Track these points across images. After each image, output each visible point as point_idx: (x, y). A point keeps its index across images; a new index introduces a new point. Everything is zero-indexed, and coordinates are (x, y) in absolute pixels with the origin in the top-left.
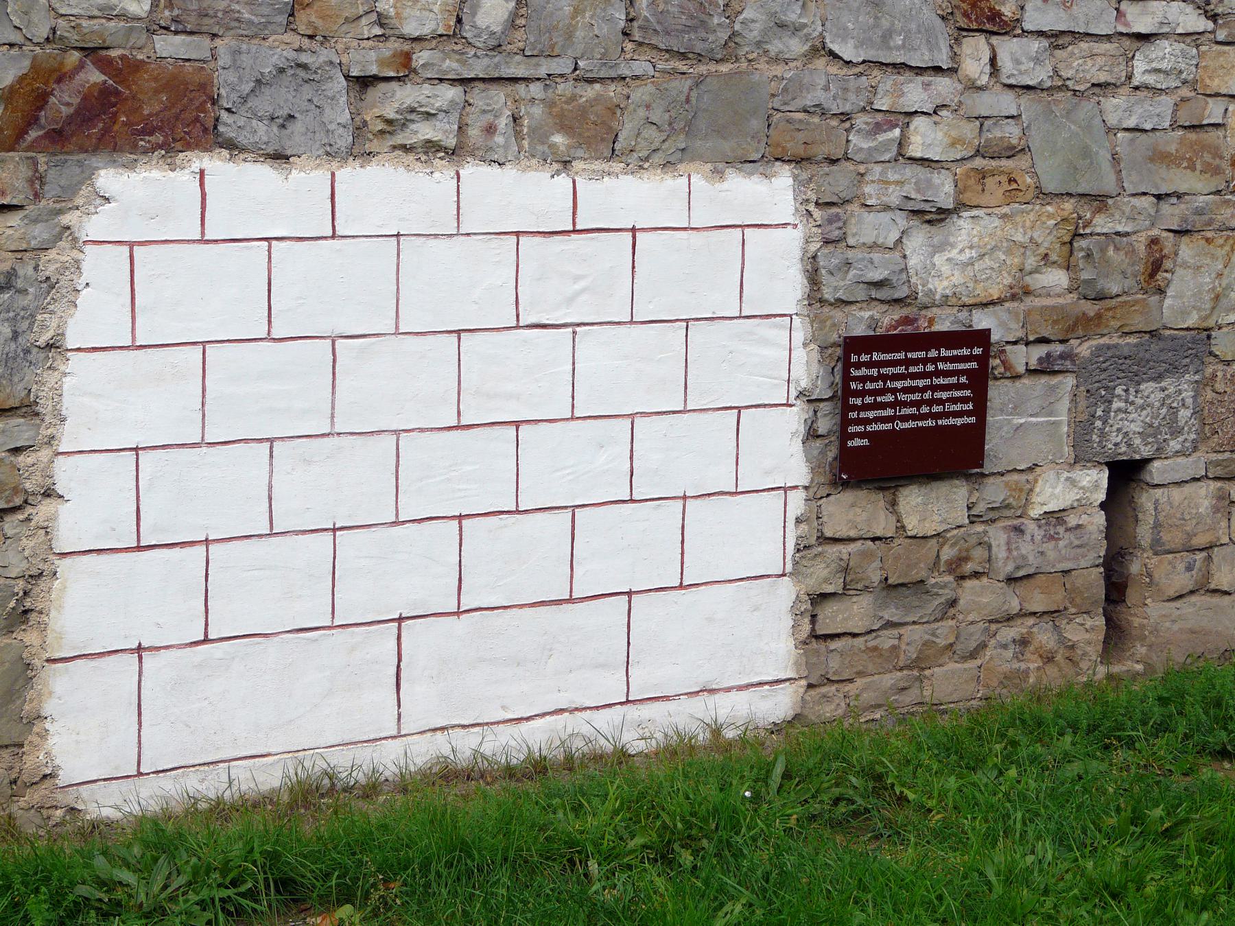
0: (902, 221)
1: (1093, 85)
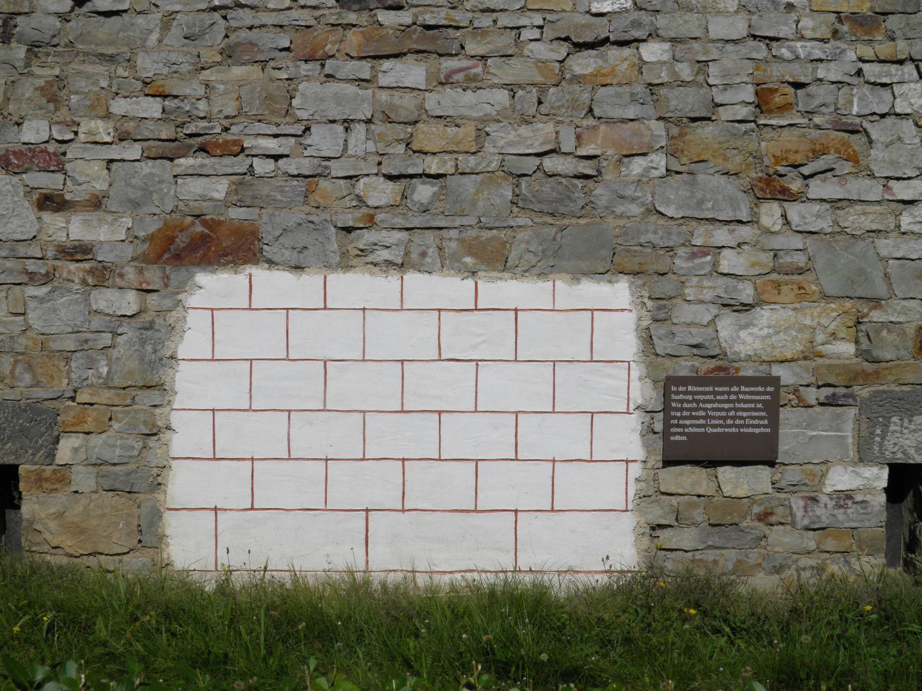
0: (714, 310)
1: (868, 231)
